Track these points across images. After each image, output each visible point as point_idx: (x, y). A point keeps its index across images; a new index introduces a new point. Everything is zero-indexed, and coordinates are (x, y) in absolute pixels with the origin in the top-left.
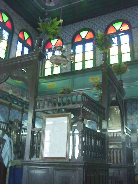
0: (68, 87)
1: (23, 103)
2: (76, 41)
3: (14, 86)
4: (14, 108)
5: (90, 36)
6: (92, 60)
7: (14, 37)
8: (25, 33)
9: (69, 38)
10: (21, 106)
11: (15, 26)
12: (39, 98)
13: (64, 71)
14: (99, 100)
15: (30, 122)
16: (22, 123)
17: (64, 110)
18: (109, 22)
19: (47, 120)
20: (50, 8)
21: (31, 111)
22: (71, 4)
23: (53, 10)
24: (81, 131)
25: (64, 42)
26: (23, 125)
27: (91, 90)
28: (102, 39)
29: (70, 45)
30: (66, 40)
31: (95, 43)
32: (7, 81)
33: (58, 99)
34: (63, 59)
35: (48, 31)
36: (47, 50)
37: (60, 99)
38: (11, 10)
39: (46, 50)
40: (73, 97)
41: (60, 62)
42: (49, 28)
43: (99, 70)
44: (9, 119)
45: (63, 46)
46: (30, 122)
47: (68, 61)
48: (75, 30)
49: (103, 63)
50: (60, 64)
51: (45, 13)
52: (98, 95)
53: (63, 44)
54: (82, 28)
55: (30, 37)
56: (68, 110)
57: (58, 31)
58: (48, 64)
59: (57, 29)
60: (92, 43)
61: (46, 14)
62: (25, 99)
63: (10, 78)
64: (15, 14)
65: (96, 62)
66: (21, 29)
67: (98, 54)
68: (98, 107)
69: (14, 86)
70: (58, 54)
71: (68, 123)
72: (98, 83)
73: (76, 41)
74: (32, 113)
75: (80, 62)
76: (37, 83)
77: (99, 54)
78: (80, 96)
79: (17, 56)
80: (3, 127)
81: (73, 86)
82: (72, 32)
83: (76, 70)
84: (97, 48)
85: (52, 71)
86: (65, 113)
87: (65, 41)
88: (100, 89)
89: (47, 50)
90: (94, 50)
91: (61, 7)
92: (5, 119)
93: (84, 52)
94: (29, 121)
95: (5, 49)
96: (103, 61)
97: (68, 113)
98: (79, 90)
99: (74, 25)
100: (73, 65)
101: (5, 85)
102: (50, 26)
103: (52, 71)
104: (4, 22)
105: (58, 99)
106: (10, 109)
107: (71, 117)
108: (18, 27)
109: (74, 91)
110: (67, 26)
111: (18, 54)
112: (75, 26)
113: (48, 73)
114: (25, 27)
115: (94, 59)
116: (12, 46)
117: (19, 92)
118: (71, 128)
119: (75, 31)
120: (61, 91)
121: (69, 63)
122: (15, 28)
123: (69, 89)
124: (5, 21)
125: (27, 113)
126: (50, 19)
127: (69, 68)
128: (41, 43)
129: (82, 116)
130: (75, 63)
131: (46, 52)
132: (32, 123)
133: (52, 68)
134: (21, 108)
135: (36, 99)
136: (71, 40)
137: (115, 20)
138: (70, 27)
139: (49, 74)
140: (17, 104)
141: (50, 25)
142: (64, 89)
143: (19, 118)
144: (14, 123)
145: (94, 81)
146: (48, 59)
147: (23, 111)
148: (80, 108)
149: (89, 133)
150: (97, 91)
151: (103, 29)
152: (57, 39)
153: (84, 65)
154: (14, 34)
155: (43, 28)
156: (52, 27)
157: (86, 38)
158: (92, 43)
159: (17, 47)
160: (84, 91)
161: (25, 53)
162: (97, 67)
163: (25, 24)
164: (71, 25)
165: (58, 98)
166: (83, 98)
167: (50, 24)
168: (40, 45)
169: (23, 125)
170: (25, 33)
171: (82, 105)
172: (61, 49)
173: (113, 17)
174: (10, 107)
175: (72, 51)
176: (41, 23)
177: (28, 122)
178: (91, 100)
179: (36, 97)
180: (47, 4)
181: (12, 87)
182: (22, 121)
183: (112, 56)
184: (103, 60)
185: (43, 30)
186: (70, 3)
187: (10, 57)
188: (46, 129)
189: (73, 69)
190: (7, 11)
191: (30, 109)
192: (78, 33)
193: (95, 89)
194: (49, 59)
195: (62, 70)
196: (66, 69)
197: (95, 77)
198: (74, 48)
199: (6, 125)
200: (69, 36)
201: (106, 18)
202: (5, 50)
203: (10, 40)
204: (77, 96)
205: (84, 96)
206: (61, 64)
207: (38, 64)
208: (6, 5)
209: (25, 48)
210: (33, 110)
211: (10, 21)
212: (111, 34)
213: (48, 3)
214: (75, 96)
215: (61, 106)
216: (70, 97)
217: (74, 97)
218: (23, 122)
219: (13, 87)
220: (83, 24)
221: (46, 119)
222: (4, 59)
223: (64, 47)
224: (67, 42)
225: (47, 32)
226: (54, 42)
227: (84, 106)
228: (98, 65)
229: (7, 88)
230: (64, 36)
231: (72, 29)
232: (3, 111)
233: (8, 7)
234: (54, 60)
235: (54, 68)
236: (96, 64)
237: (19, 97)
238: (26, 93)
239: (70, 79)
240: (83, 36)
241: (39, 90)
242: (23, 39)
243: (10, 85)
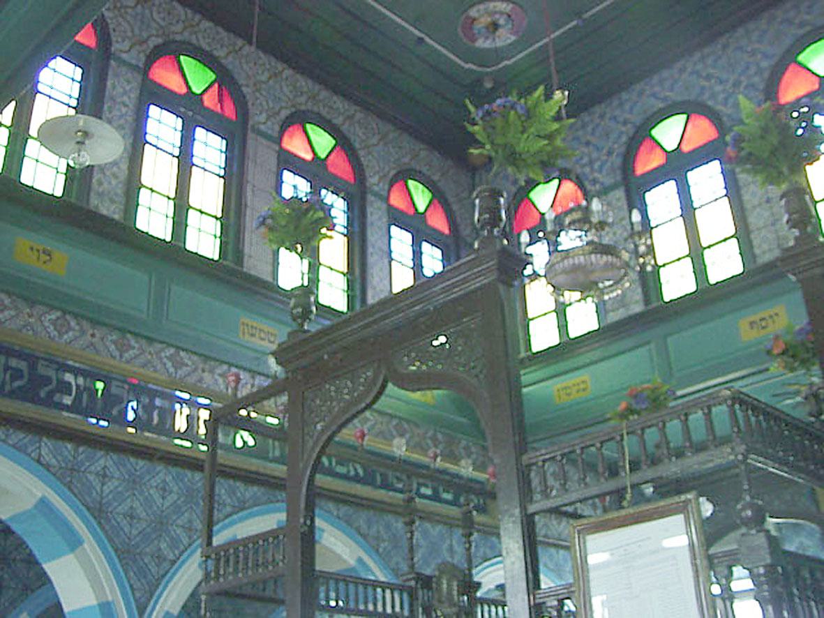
0: (649, 381)
1: (462, 487)
2: (640, 170)
3: (408, 421)
4: (428, 517)
5: (702, 131)
6: (734, 240)
8: (411, 183)
10: (454, 503)
12: (539, 453)
13: (613, 317)
14: (811, 415)
15: (513, 563)
16: (471, 575)
17: (649, 490)
18: (778, 51)
19: (589, 544)
20: (498, 54)
21: (512, 515)
22: (586, 16)
23: (514, 60)
24: (762, 571)
25: (589, 187)
26: (479, 585)
27: (761, 377)
28: (765, 130)
29: (620, 194)
30: (596, 175)
31: (737, 157)
32: (382, 403)
33: (625, 443)
34: (605, 258)
35: (518, 149)
36: (525, 237)
37: (634, 439)
38: (339, 103)
39: (519, 235)
40: (691, 417)
41: (593, 277)
42: (520, 135)
43: (782, 276)
44: (412, 566)
45: (589, 203)
46: (513, 563)
47: (627, 265)
48: (625, 123)
49: (796, 239)
50: (596, 284)
51: (479, 81)
52: (797, 393)
53: (587, 196)
54: (655, 109)
55: (439, 197)
56: (670, 488)
57: (558, 142)
58: (538, 297)
59: (552, 132)
60: (715, 166)
61: (488, 85)
62: (466, 469)
63: (394, 384)
64: (359, 116)
65: (755, 243)
66: (393, 172)
67: (754, 207)
68: (816, 447)
69: (408, 421)
70: (578, 243)
71: (691, 545)
72: (788, 338)
73: (640, 170)
74: (519, 520)
75: (725, 240)
76: (514, 387)
77: (760, 204)
78: (724, 408)
79: (397, 289)
80: (393, 607)
81: (671, 375)
82: (613, 136)
83: (667, 299)
84: (743, 177)
85: (563, 326)
86: (656, 500)
87: (595, 181)
88: (804, 362)
89: (525, 237)
90: (733, 191)
91: (545, 41)
92: (396, 572)
93: (688, 211)
94: (508, 562)
95: (343, 267)
96: (796, 232)
97: (683, 497)
98: (702, 386)
99: (616, 103)
100: (650, 281)
101: (369, 424)
102: (520, 129)
103: (563, 326)
104: (319, 158)
105: (622, 440)
106: (413, 522)
107: (699, 511)
108: (382, 165)
109: (679, 393)
110: (585, 117)
111: (402, 279)
112: (621, 105)
113: (543, 336)
114: (406, 160)
115: (743, 234)
116: (370, 250)
117: (436, 442)
118: (711, 566)
119: (629, 126)
120: (623, 405)
121: (633, 275)
122: (368, 173)
123: (654, 390)
124: (323, 155)
125: (493, 532)
126: (513, 98)
127: (638, 295)
128: (499, 211)
129: (752, 498)
130: (657, 267)
131: (523, 247)
132: (524, 569)
133: (561, 311)
134: (454, 511)
135: (525, 459)
136: (619, 172)
137: (801, 32)
138: (602, 117)
139: (689, 286)
140: (436, 497)
141: (519, 123)
142: (636, 396)
143: (452, 557)
144: (439, 584)
145: (763, 332)
146: (535, 276)
147: (468, 525)
148: (732, 465)
149: (804, 580)
150: (792, 374)
151: (757, 90)
152: (556, 182)
153: (700, 270)
154: (370, 198)
155: (492, 143)
156: (532, 130)
157: (686, 148)
158: (715, 166)
159: (391, 251)
160: (740, 383)
161: (428, 272)
162: (770, 265)
163: (407, 149)
164: (642, 83)
165: (622, 436)
166: (739, 414)
167: (519, 117)
168: (495, 220)
169: (479, 585)
170: (411, 183)
171: (742, 448)
172: (584, 221)
173: (789, 22)
174: (410, 514)
175: (636, 216)
176: (480, 122)
177: (504, 567)
178: (776, 419)
179: (522, 447)
180: (482, 43)
181: (402, 424)
182: (470, 569)
183: (664, 265)
184: (792, 224)
185: (497, 152)
186: (578, 14)
187: (371, 300)
188: (592, 584)
189: (653, 298)
190: (324, 112)
191: (506, 507)
192: (641, 136)
193: (775, 367)
194: (542, 272)
195: (606, 312)
196: (622, 301)
197: (765, 314)
198: (635, 200)
199: (405, 596)
200: (604, 158)
201: (755, 36)
202: (342, 273)
203: (357, 229)
204: (710, 411)
205: (742, 402)
206: (601, 285)
207: (502, 306)
209: (426, 247)
210: (517, 511)
211: (343, 148)
212: (804, 100)
213: (487, 38)
214: (700, 413)
215: (645, 467)
216: (676, 422)
217: (674, 427)
218: (474, 572)
219: (406, 426)
220: (699, 67)
221: (584, 538)
222: (345, 310)
223: (596, 205)
224: (602, 184)
225: (514, 158)
226: (543, 197)
227: (748, 451)
228: (767, 253)
229: (380, 434)
230: (585, 160)
231: (612, 124)
232: (378, 538)
233: (324, 94)
234: (564, 271)
235: (568, 310)
236: (757, 251)
237: (439, 463)
239: (648, 343)
240: (670, 143)
241: (529, 419)
242: (411, 211)
243: (392, 416)
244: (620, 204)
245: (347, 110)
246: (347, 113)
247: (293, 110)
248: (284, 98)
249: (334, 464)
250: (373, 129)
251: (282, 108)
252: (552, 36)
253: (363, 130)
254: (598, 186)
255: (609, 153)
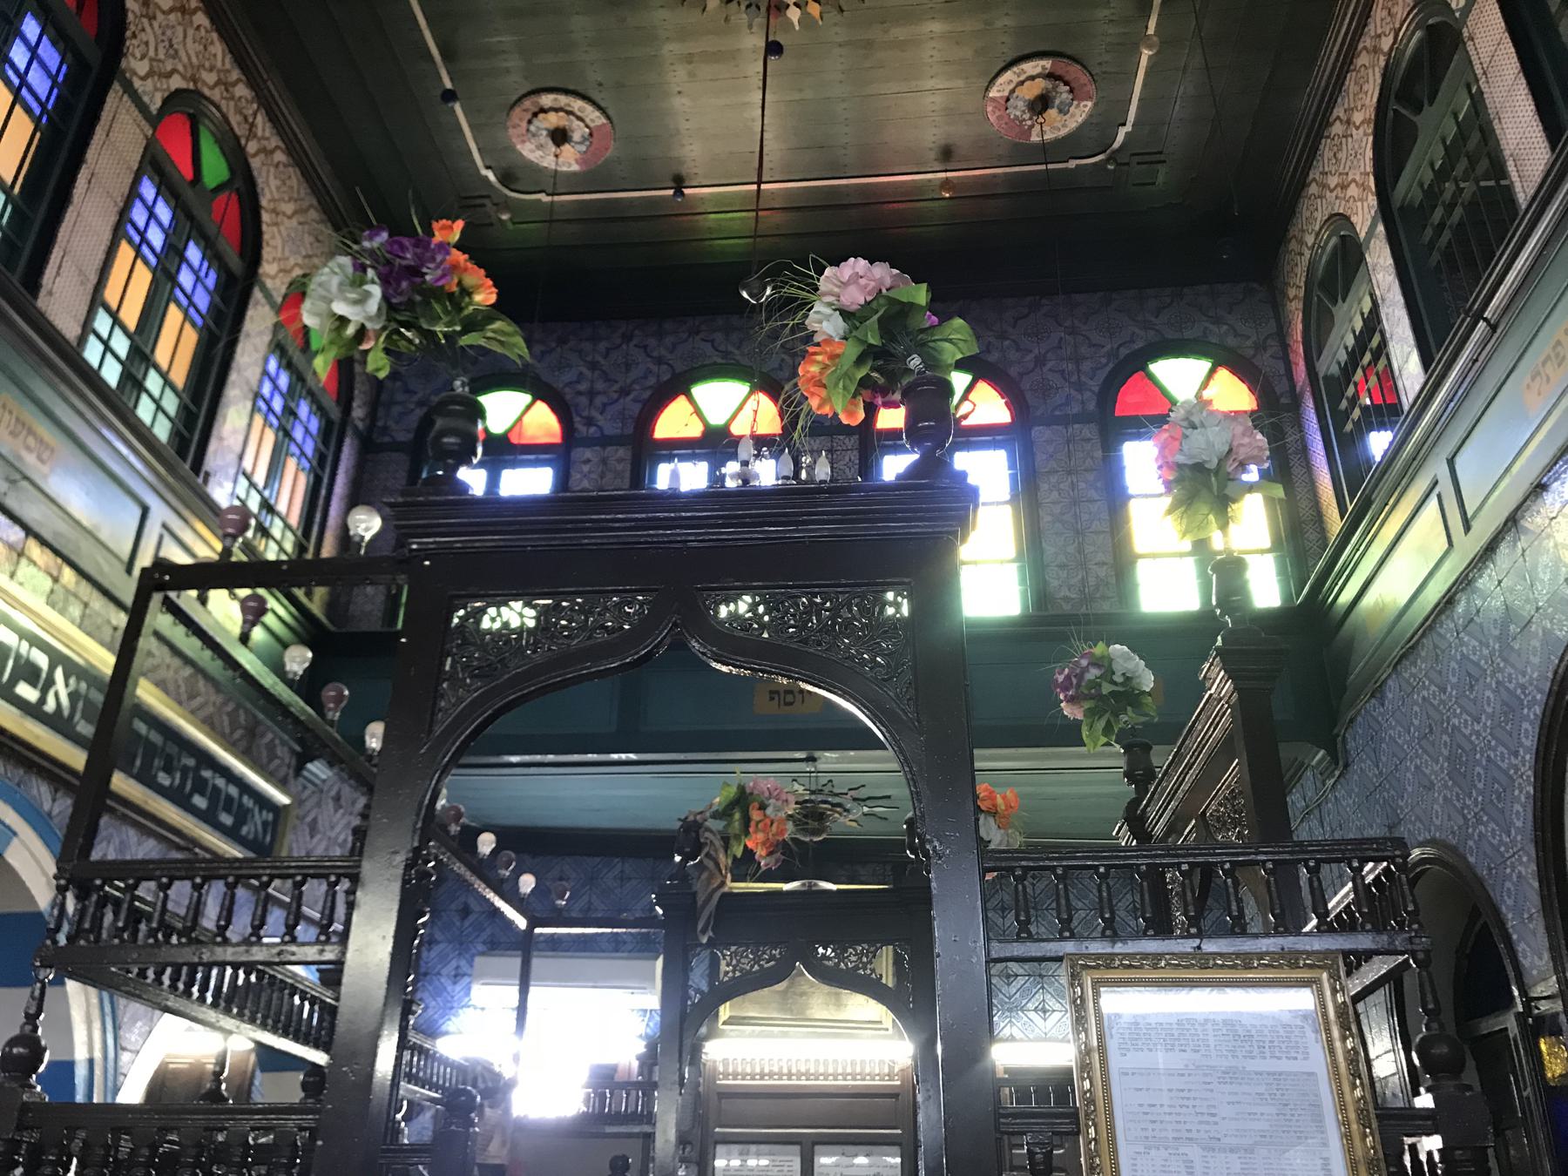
7: (250, 313)
9: (618, 407)
11: (266, 237)
48: (660, 361)
64: (280, 157)
87: (590, 422)
122: (267, 253)
154: (257, 294)
208: (236, 74)
213: (540, 147)
238: (270, 736)
244: (620, 467)
245: (267, 139)
246: (265, 143)
247: (191, 86)
248: (182, 54)
249: (78, 716)
250: (292, 187)
251: (174, 71)
252: (1050, 166)
253: (278, 183)
254: (593, 429)
255: (624, 392)
